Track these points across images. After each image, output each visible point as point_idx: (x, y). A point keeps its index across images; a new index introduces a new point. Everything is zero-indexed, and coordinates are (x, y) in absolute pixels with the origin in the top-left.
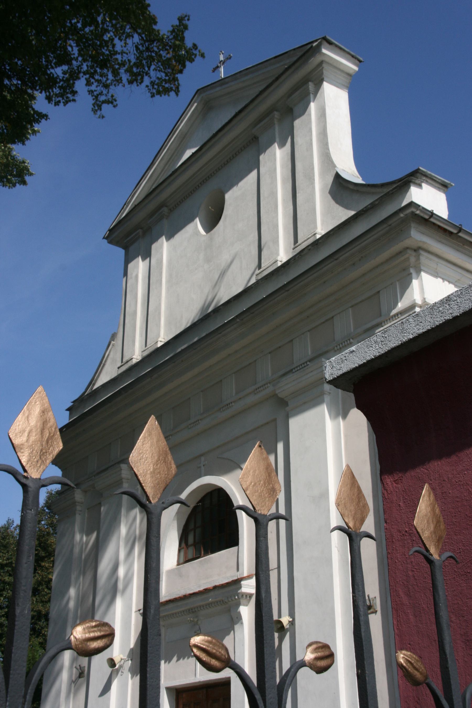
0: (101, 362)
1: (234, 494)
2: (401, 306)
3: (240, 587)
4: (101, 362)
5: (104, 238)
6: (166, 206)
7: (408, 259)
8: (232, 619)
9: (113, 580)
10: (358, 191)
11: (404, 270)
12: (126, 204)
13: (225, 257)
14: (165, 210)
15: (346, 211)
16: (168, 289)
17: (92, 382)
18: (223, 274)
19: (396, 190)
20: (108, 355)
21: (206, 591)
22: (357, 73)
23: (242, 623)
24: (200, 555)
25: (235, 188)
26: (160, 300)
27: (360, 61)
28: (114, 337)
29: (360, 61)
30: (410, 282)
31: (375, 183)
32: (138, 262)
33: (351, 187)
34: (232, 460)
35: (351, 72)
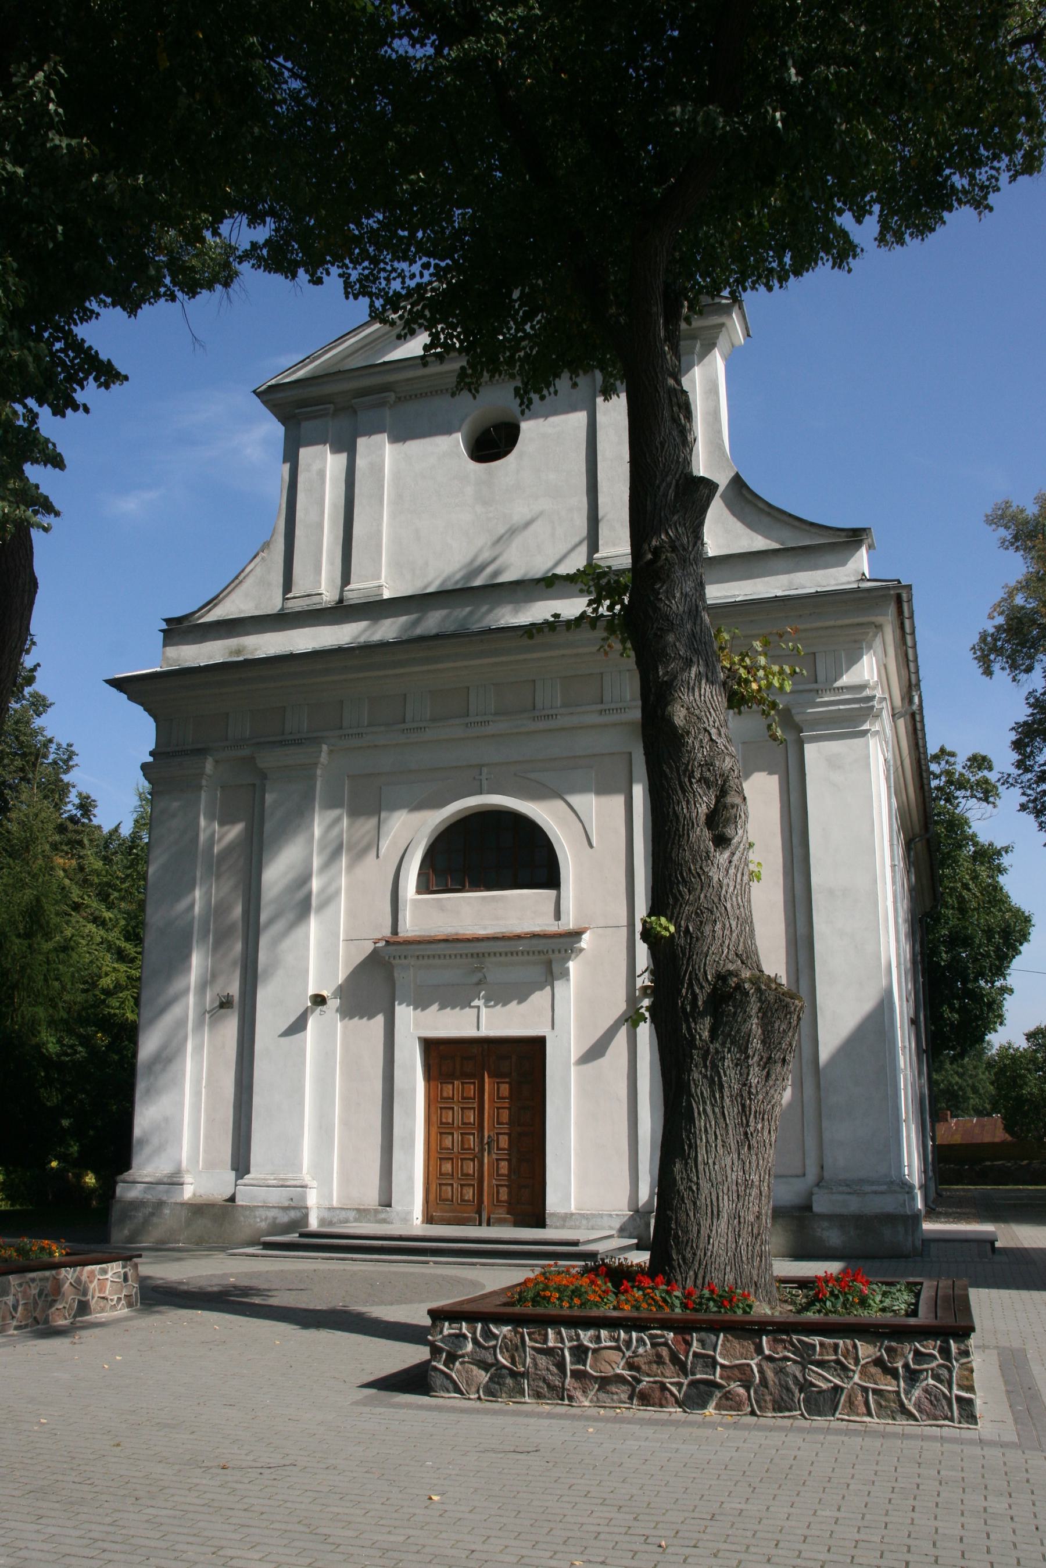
0: (237, 578)
1: (552, 828)
2: (845, 680)
3: (580, 941)
4: (237, 578)
5: (254, 392)
6: (395, 392)
7: (868, 633)
8: (551, 973)
9: (301, 894)
10: (769, 514)
11: (855, 641)
12: (310, 358)
13: (520, 511)
14: (392, 397)
15: (738, 526)
16: (393, 516)
17: (213, 602)
18: (513, 532)
19: (766, 509)
20: (247, 575)
21: (519, 937)
22: (740, 346)
23: (568, 980)
24: (464, 886)
25: (541, 420)
26: (380, 525)
27: (749, 335)
28: (266, 546)
29: (749, 335)
30: (859, 658)
31: (805, 518)
32: (382, 448)
33: (761, 505)
34: (544, 785)
35: (737, 344)
